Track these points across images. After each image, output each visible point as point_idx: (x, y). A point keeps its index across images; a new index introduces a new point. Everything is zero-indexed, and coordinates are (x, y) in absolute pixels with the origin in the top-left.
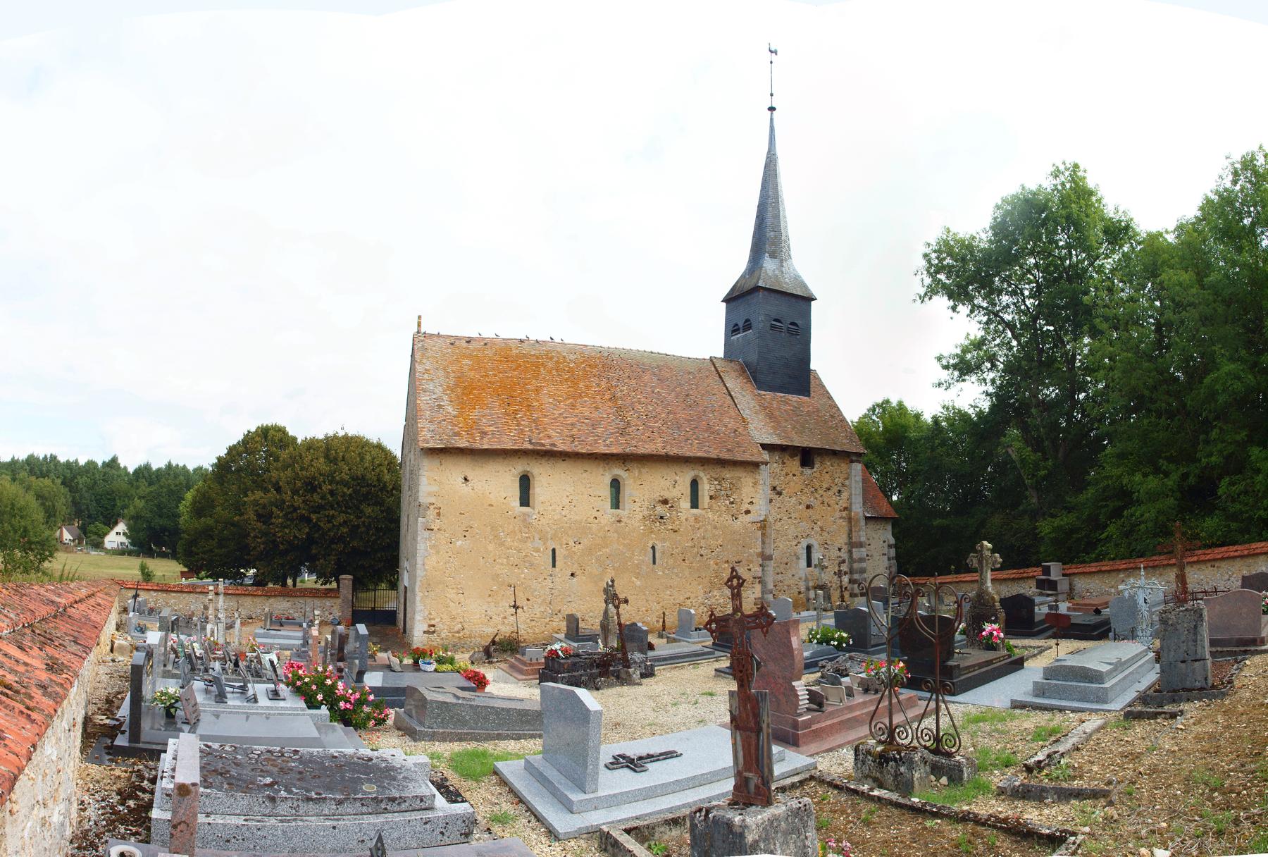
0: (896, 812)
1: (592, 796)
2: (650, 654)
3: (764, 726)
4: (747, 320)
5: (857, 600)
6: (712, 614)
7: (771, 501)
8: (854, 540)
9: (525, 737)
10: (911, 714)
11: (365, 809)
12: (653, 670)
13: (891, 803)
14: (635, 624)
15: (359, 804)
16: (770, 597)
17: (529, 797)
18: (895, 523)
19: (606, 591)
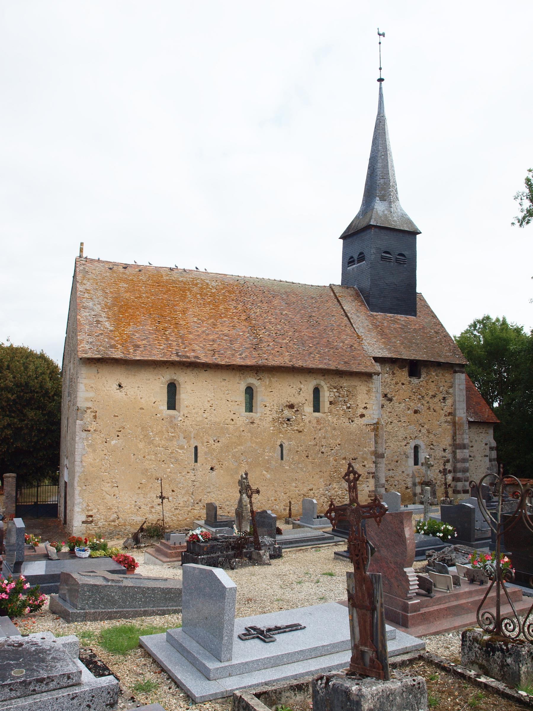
0: (503, 702)
1: (227, 664)
2: (278, 537)
3: (378, 605)
4: (361, 253)
5: (459, 496)
6: (332, 504)
7: (383, 406)
8: (458, 442)
9: (169, 612)
10: (518, 607)
11: (13, 694)
12: (280, 552)
13: (496, 691)
14: (265, 512)
15: (7, 690)
16: (383, 491)
17: (169, 666)
18: (496, 427)
19: (240, 483)
